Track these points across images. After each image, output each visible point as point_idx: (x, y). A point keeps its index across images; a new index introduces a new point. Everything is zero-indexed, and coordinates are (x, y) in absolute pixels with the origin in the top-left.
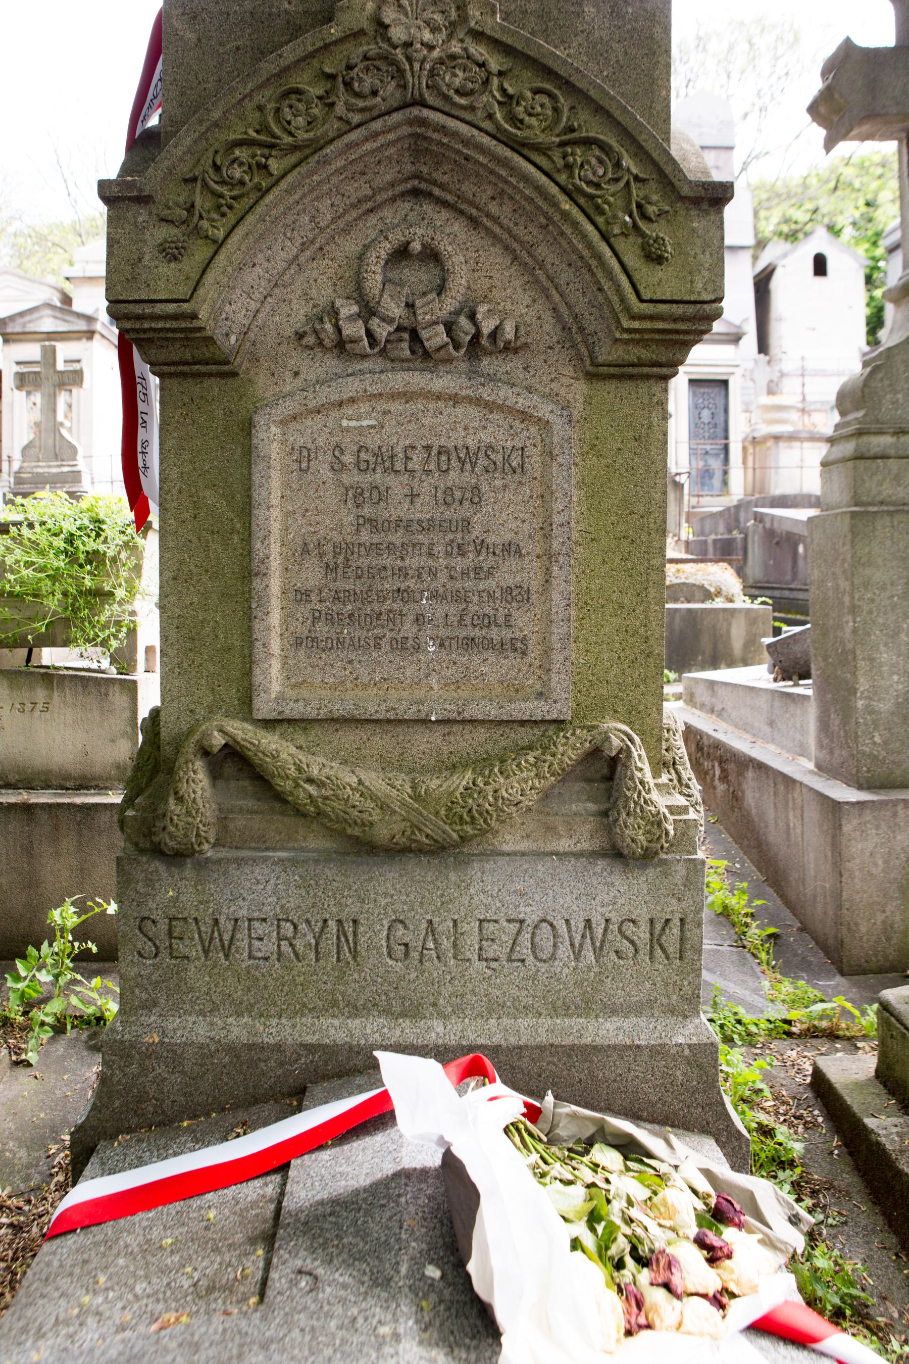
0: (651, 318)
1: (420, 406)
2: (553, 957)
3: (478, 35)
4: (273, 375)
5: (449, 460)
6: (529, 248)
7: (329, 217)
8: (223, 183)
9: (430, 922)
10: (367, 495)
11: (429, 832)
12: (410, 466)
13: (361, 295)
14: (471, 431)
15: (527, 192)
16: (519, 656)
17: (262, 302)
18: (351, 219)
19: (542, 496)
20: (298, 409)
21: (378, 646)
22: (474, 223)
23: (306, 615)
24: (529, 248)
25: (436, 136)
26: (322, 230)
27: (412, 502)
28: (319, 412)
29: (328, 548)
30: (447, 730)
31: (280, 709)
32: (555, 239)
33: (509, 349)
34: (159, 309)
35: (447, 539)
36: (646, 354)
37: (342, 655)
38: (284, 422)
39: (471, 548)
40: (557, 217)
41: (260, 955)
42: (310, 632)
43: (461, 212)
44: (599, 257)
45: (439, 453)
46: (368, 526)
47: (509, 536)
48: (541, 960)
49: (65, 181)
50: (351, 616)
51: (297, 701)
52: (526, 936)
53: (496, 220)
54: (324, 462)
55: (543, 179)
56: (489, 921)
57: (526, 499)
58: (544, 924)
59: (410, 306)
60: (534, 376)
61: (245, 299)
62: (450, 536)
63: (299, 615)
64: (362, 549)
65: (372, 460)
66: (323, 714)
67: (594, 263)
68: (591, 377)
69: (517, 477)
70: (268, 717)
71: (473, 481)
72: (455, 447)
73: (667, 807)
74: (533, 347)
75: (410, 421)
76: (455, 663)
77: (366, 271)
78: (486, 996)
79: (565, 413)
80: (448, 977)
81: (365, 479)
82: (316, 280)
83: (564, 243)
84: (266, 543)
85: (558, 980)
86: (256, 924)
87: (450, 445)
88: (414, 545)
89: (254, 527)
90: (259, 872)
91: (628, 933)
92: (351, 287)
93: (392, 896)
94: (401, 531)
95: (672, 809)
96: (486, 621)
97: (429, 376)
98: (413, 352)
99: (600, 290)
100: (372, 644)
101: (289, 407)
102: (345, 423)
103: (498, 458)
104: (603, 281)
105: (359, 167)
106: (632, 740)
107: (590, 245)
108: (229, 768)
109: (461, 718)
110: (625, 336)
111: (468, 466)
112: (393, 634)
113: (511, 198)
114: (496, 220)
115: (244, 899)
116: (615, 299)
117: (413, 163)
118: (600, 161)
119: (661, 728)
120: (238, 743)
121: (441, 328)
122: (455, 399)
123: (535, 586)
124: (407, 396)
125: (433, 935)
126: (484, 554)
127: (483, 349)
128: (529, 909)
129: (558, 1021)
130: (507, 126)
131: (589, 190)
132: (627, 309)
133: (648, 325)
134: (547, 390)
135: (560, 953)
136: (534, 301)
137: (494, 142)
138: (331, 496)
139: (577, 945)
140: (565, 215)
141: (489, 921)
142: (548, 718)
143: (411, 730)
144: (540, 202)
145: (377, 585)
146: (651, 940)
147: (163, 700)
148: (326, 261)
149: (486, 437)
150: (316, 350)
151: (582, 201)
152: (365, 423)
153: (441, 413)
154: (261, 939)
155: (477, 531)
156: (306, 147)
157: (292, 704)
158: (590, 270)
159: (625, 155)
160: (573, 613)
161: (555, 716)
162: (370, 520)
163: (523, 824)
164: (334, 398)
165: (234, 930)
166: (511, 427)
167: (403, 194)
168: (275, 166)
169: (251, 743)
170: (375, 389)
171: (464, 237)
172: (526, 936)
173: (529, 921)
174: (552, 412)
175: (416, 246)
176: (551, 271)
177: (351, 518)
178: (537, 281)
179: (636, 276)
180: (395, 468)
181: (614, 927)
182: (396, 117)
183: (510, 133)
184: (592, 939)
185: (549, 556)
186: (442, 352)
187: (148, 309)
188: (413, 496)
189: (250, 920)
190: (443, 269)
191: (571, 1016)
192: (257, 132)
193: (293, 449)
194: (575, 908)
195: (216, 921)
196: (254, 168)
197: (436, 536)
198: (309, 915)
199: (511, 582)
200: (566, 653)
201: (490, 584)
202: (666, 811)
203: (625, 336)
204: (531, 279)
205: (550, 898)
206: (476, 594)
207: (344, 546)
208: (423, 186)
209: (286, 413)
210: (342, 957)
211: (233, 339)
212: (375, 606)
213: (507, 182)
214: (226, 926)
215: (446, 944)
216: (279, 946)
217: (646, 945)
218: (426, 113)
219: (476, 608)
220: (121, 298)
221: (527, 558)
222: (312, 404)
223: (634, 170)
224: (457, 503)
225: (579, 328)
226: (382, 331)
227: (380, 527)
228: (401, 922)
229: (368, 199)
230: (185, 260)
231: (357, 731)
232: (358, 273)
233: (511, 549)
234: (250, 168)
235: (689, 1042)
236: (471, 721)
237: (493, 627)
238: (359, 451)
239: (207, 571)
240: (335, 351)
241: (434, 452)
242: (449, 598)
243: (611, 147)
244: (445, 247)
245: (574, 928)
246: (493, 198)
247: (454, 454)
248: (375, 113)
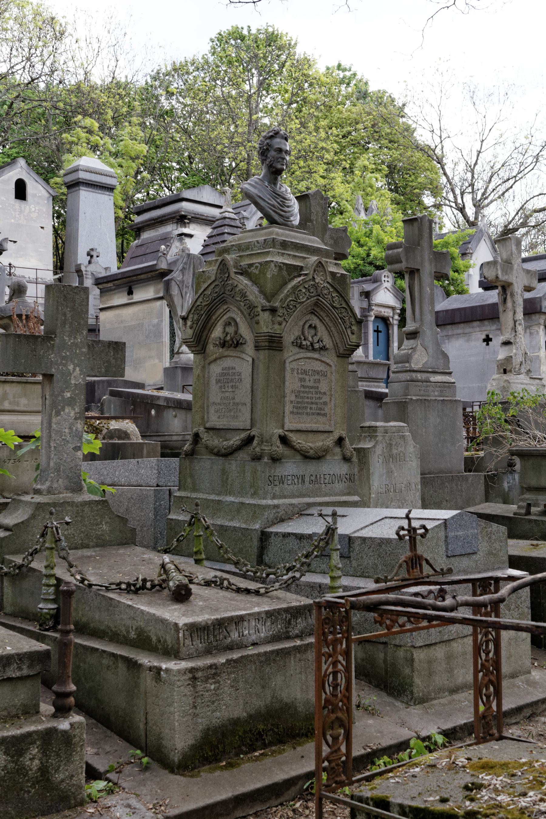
3: (328, 283)
22: (321, 320)
68: (338, 356)
101: (291, 359)
122: (317, 359)
123: (328, 402)
124: (309, 358)
138: (297, 379)
149: (321, 368)
168: (297, 306)
185: (331, 395)
201: (321, 401)
233: (325, 393)
244: (318, 326)
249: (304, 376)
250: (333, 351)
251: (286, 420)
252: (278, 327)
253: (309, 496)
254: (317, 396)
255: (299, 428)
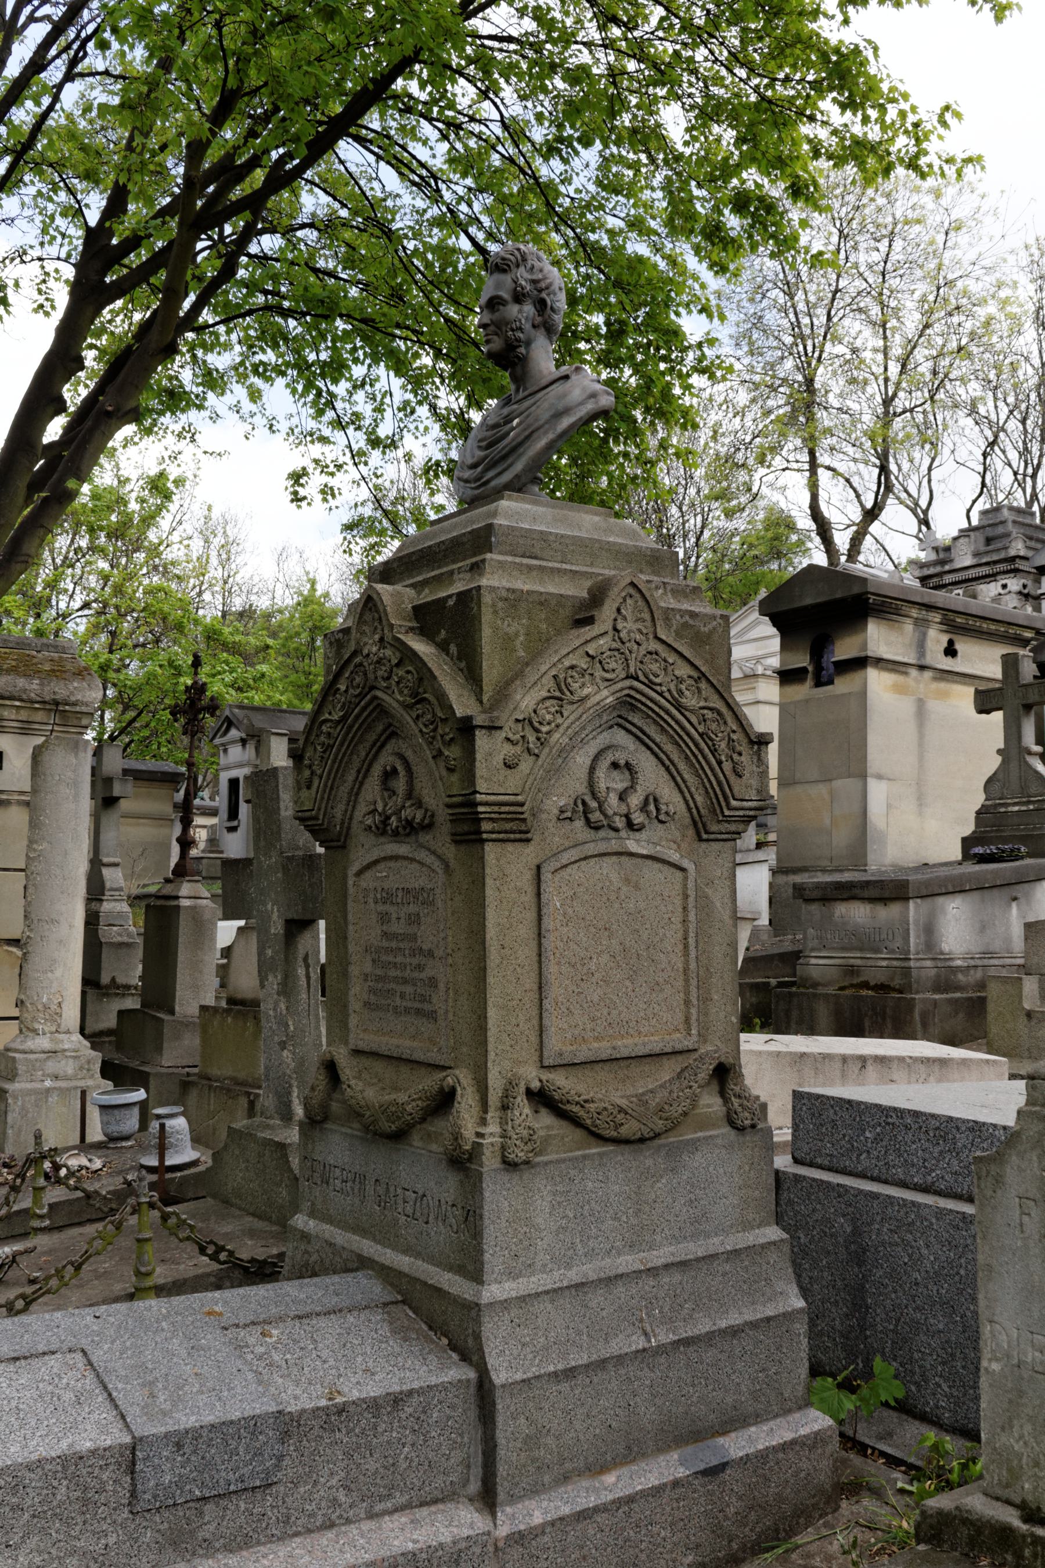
68: (456, 842)
249: (387, 908)
251: (353, 1021)
254: (415, 961)
255: (374, 1047)
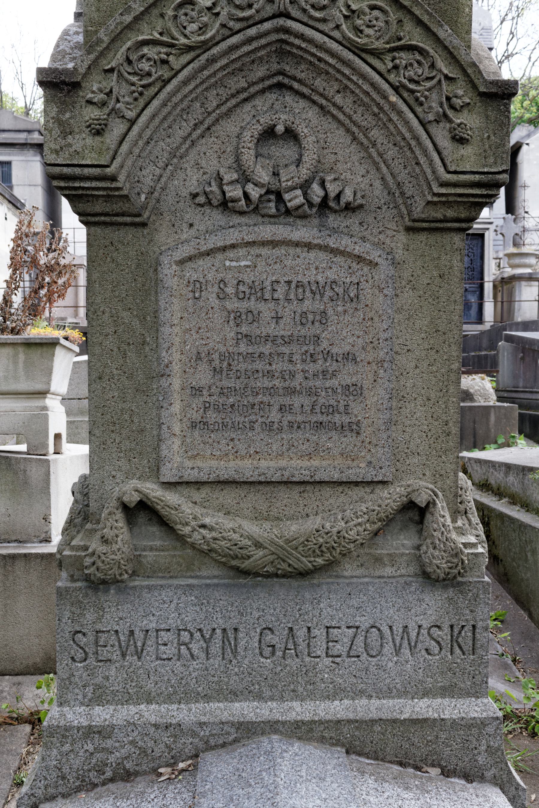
0: (455, 185)
1: (283, 252)
2: (380, 653)
4: (173, 225)
5: (304, 291)
6: (365, 131)
7: (215, 104)
8: (135, 74)
9: (291, 629)
10: (244, 317)
11: (291, 562)
12: (276, 296)
13: (240, 166)
14: (321, 270)
15: (365, 87)
16: (354, 435)
17: (164, 169)
18: (231, 106)
19: (372, 319)
20: (193, 252)
21: (252, 429)
23: (199, 406)
24: (365, 131)
25: (297, 42)
26: (209, 114)
27: (277, 323)
28: (208, 255)
29: (216, 356)
30: (302, 489)
31: (181, 474)
32: (385, 124)
33: (349, 208)
34: (87, 171)
35: (303, 350)
36: (450, 213)
37: (226, 435)
38: (181, 262)
39: (321, 356)
40: (386, 107)
41: (165, 656)
42: (202, 418)
43: (314, 102)
44: (417, 138)
45: (297, 286)
46: (245, 340)
47: (348, 348)
48: (372, 656)
49: (25, 97)
50: (232, 406)
51: (193, 468)
52: (360, 639)
53: (340, 108)
54: (213, 293)
55: (377, 78)
56: (334, 628)
57: (360, 321)
58: (374, 630)
59: (276, 174)
60: (367, 229)
61: (152, 167)
62: (305, 348)
63: (194, 405)
64: (241, 357)
65: (248, 291)
66: (212, 478)
67: (413, 143)
68: (409, 229)
69: (354, 305)
70: (173, 480)
71: (322, 307)
72: (309, 282)
73: (462, 543)
74: (366, 208)
75: (276, 263)
76: (308, 440)
77: (243, 147)
78: (332, 683)
79: (390, 257)
80: (304, 669)
81: (243, 306)
82: (205, 154)
83: (391, 127)
84: (170, 352)
85: (384, 670)
86: (162, 633)
87: (305, 281)
88: (279, 355)
89: (161, 340)
90: (165, 595)
91: (435, 636)
92: (231, 160)
93: (263, 610)
94: (269, 344)
95: (465, 545)
96: (331, 410)
97: (289, 228)
98: (278, 210)
99: (418, 164)
100: (248, 426)
102: (228, 263)
103: (340, 291)
104: (419, 157)
105: (238, 65)
106: (436, 495)
107: (411, 130)
108: (142, 517)
109: (313, 480)
110: (436, 199)
111: (318, 297)
112: (263, 420)
113: (353, 92)
114: (340, 108)
115: (153, 615)
116: (428, 171)
117: (278, 63)
118: (419, 62)
119: (457, 487)
120: (149, 499)
121: (299, 192)
122: (309, 246)
124: (273, 244)
125: (293, 639)
126: (330, 361)
127: (330, 208)
128: (363, 618)
129: (385, 702)
130: (351, 36)
131: (412, 86)
132: (437, 179)
133: (453, 191)
134: (376, 240)
135: (385, 651)
136: (368, 172)
137: (341, 48)
138: (218, 318)
139: (398, 645)
140: (393, 106)
141: (334, 628)
142: (375, 480)
143: (276, 489)
144: (374, 95)
145: (252, 383)
146: (452, 641)
147: (91, 468)
148: (213, 139)
149: (331, 275)
150: (205, 207)
151: (405, 95)
152: (243, 263)
153: (298, 257)
154: (165, 645)
155: (325, 344)
156: (198, 47)
157: (189, 470)
158: (410, 148)
159: (439, 60)
160: (394, 404)
161: (380, 478)
162: (246, 336)
163: (358, 556)
164: (220, 244)
165: (145, 639)
166: (350, 268)
167: (270, 88)
168: (176, 62)
169: (160, 500)
170: (249, 238)
171: (316, 122)
172: (360, 639)
173: (363, 627)
174: (380, 256)
175: (280, 129)
176: (381, 149)
177: (232, 334)
178: (370, 156)
179: (445, 153)
180: (265, 298)
181: (424, 632)
182: (267, 25)
183: (354, 41)
184: (409, 640)
186: (300, 211)
187: (77, 171)
188: (278, 319)
189: (157, 631)
190: (300, 146)
191: (393, 698)
192: (161, 34)
193: (189, 282)
194: (396, 617)
195: (132, 633)
196: (158, 63)
197: (295, 348)
198: (202, 626)
199: (349, 382)
200: (389, 433)
201: (334, 383)
202: (461, 546)
203: (436, 199)
204: (365, 155)
205: (378, 611)
206: (324, 390)
207: (227, 355)
208: (286, 81)
209: (184, 255)
210: (226, 656)
211: (143, 197)
212: (251, 399)
213: (349, 79)
214: (139, 635)
215: (303, 646)
216: (179, 650)
217: (447, 644)
218: (290, 23)
219: (324, 400)
220: (56, 162)
221: (361, 365)
222: (203, 249)
223: (446, 72)
224: (310, 323)
225: (401, 193)
226: (255, 193)
227: (253, 340)
228: (270, 629)
229: (244, 90)
230: (107, 135)
231: (237, 490)
232: (237, 148)
234: (155, 63)
235: (480, 716)
236: (320, 483)
237: (336, 415)
238: (238, 284)
239: (125, 373)
240: (221, 209)
241: (293, 285)
242: (304, 393)
243: (428, 53)
244: (302, 130)
245: (395, 632)
246: (338, 92)
247: (308, 288)
248: (251, 22)
250: (387, 214)
252: (89, 141)
253: (260, 697)
